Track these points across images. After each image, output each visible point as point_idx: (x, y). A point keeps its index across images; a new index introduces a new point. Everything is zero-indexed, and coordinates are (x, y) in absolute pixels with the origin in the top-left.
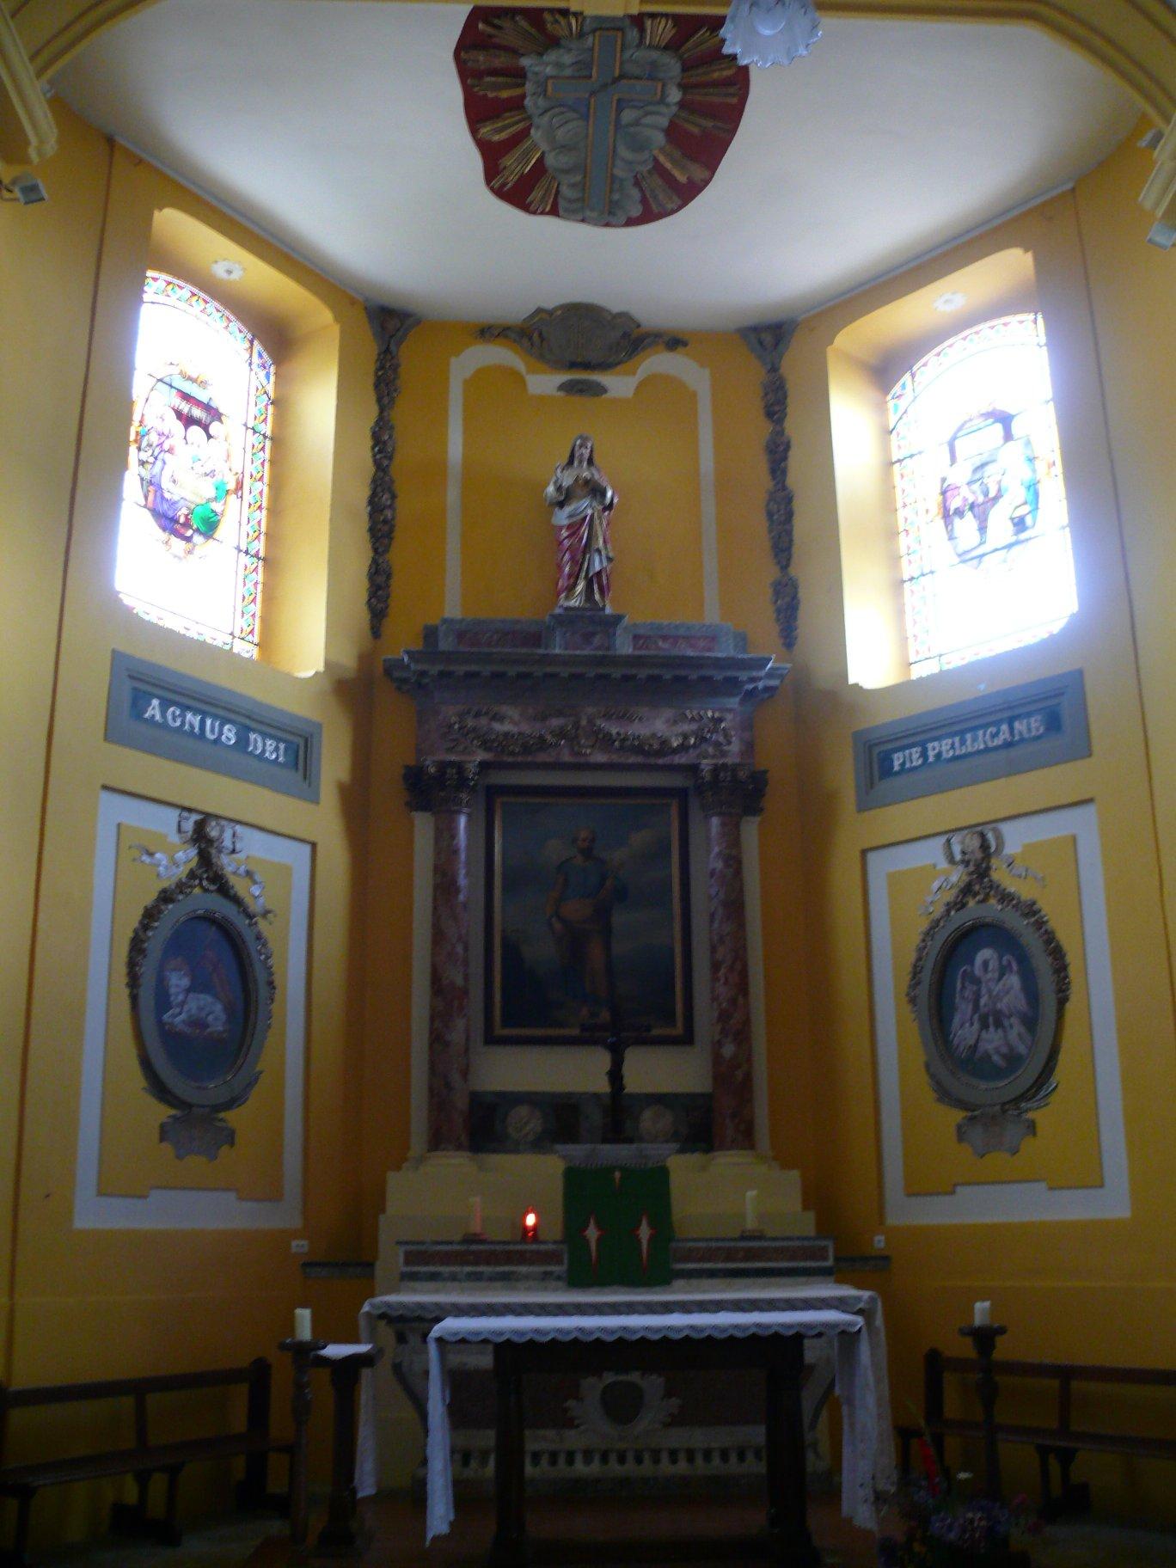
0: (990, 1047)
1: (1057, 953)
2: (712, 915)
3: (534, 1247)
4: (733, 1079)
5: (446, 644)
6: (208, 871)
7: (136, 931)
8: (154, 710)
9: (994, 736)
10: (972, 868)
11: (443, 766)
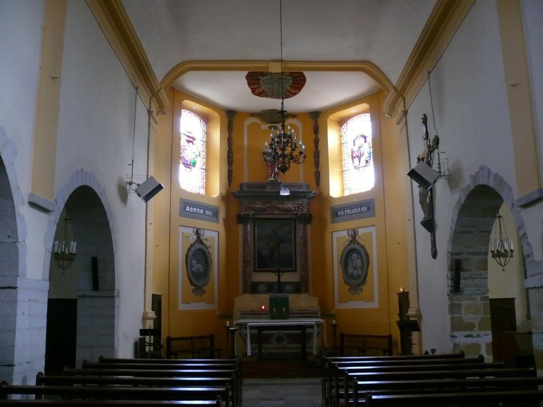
1: (367, 255)
5: (245, 189)
6: (199, 240)
8: (188, 209)
11: (244, 215)
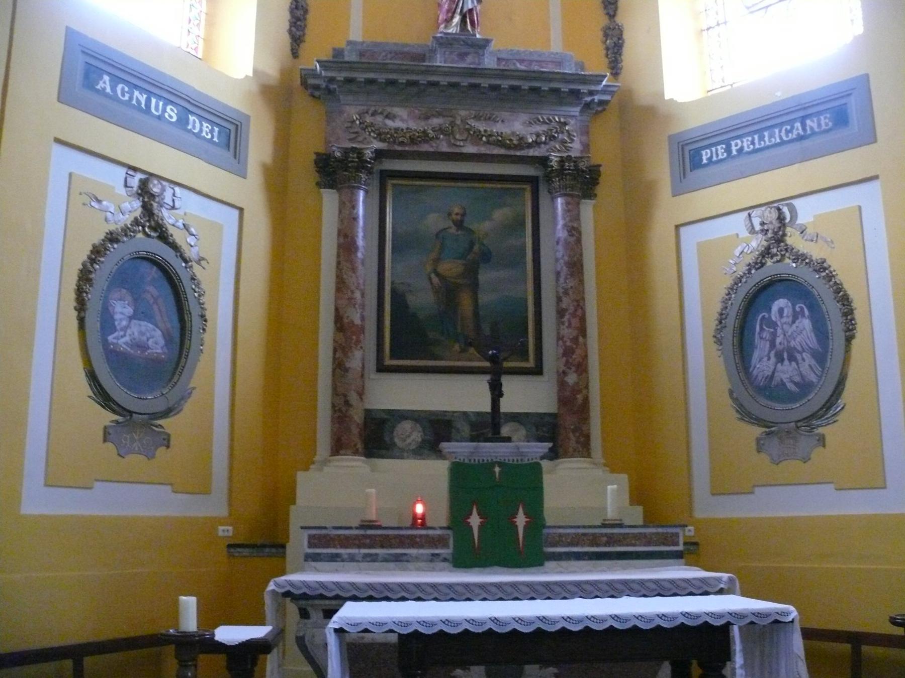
0: (785, 377)
1: (845, 300)
2: (558, 274)
3: (423, 532)
4: (573, 402)
7: (84, 265)
8: (105, 83)
9: (788, 132)
10: (770, 235)
11: (346, 151)
